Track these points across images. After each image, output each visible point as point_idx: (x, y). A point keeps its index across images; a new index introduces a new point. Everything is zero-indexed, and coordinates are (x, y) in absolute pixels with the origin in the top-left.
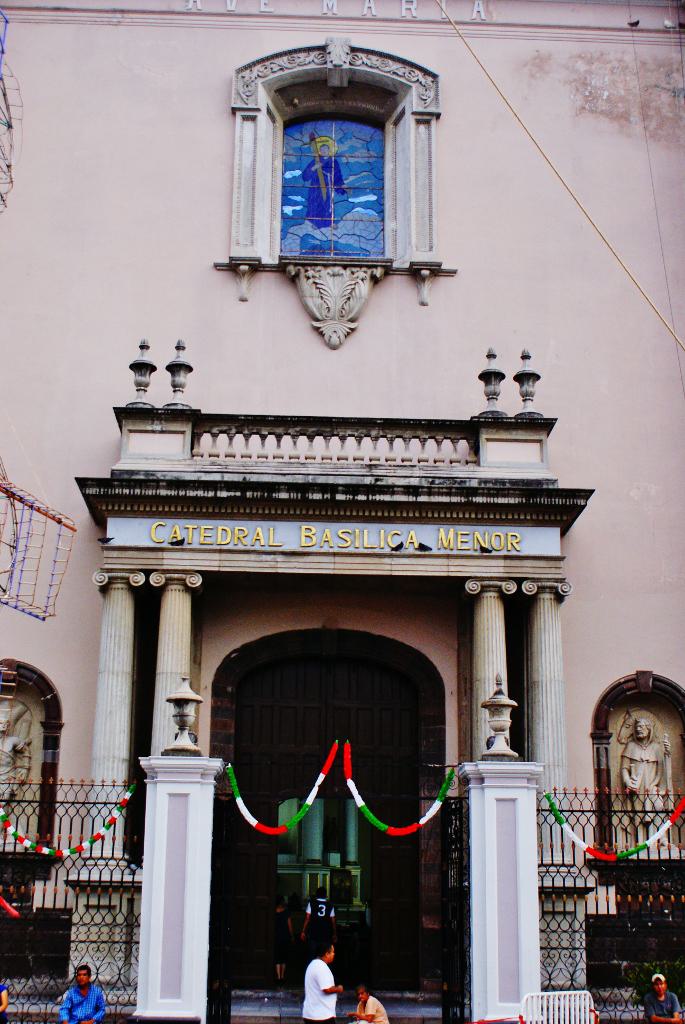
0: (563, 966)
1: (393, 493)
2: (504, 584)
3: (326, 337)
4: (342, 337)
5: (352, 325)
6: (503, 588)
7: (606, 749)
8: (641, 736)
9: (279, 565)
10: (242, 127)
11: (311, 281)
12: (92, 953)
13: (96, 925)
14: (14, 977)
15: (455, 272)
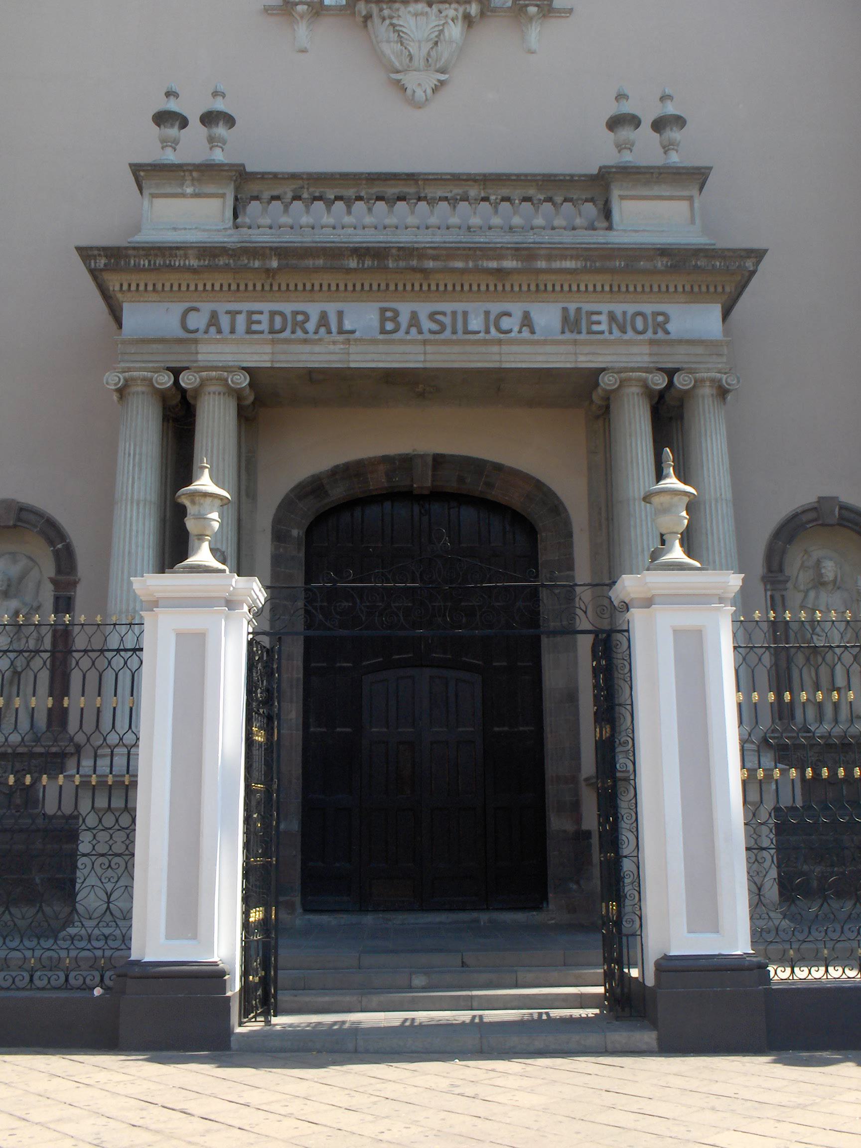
0: (87, 923)
1: (500, 257)
2: (650, 376)
3: (409, 92)
4: (429, 91)
5: (443, 77)
6: (724, 382)
7: (783, 597)
8: (826, 579)
9: (352, 357)
10: (617, 230)
11: (387, 22)
12: (99, 871)
13: (106, 829)
14: (249, 915)
15: (571, 11)
